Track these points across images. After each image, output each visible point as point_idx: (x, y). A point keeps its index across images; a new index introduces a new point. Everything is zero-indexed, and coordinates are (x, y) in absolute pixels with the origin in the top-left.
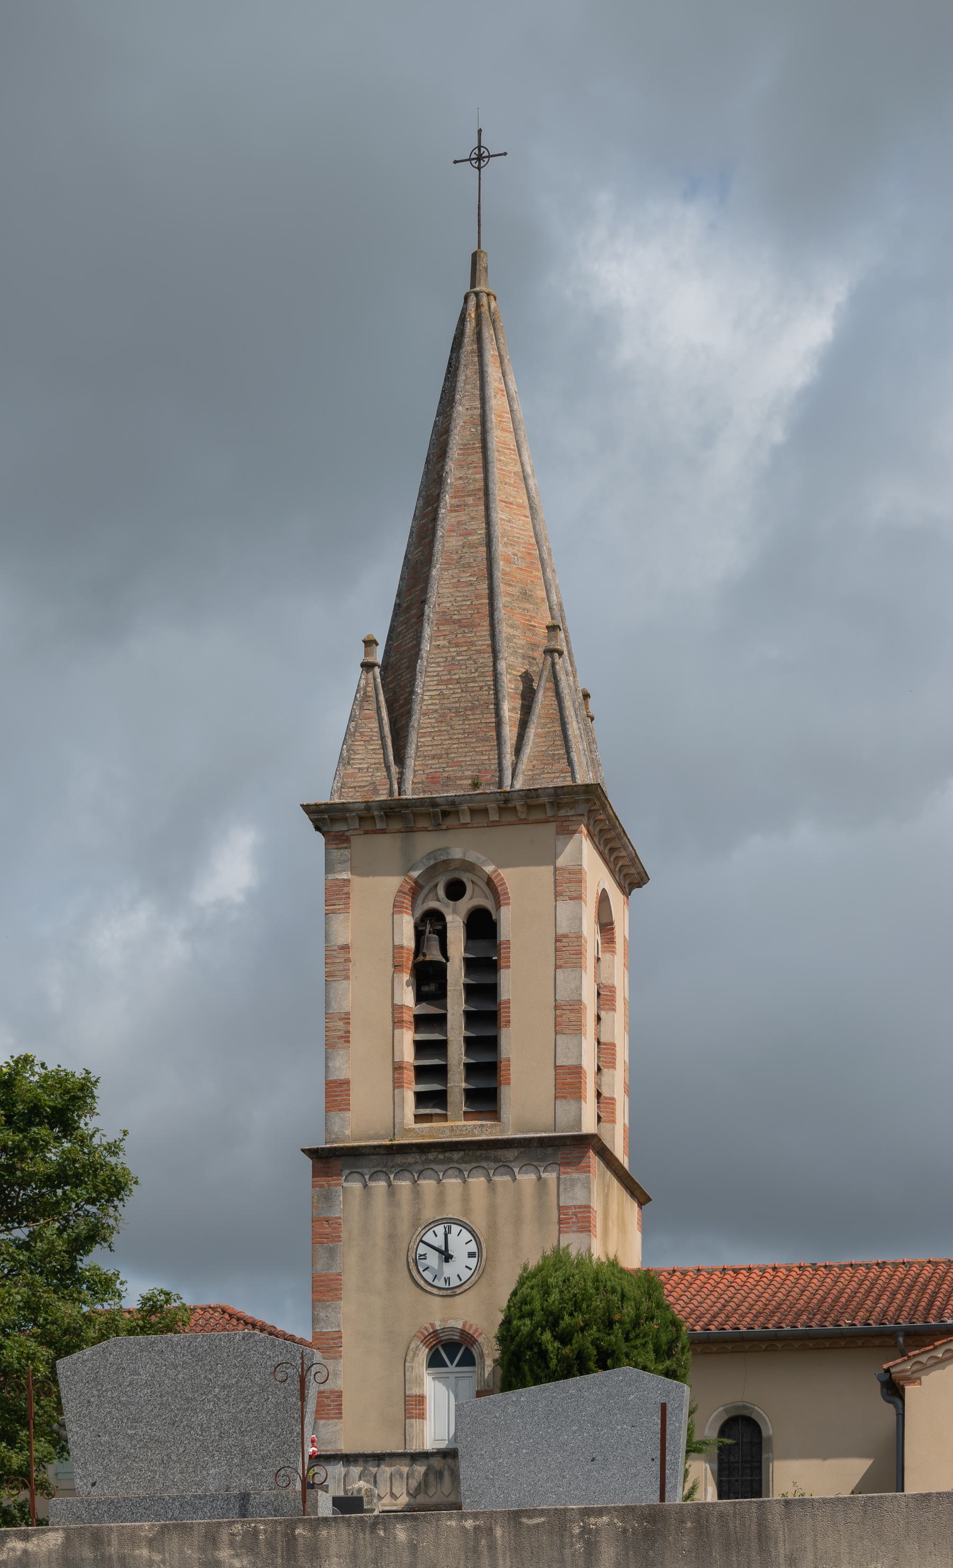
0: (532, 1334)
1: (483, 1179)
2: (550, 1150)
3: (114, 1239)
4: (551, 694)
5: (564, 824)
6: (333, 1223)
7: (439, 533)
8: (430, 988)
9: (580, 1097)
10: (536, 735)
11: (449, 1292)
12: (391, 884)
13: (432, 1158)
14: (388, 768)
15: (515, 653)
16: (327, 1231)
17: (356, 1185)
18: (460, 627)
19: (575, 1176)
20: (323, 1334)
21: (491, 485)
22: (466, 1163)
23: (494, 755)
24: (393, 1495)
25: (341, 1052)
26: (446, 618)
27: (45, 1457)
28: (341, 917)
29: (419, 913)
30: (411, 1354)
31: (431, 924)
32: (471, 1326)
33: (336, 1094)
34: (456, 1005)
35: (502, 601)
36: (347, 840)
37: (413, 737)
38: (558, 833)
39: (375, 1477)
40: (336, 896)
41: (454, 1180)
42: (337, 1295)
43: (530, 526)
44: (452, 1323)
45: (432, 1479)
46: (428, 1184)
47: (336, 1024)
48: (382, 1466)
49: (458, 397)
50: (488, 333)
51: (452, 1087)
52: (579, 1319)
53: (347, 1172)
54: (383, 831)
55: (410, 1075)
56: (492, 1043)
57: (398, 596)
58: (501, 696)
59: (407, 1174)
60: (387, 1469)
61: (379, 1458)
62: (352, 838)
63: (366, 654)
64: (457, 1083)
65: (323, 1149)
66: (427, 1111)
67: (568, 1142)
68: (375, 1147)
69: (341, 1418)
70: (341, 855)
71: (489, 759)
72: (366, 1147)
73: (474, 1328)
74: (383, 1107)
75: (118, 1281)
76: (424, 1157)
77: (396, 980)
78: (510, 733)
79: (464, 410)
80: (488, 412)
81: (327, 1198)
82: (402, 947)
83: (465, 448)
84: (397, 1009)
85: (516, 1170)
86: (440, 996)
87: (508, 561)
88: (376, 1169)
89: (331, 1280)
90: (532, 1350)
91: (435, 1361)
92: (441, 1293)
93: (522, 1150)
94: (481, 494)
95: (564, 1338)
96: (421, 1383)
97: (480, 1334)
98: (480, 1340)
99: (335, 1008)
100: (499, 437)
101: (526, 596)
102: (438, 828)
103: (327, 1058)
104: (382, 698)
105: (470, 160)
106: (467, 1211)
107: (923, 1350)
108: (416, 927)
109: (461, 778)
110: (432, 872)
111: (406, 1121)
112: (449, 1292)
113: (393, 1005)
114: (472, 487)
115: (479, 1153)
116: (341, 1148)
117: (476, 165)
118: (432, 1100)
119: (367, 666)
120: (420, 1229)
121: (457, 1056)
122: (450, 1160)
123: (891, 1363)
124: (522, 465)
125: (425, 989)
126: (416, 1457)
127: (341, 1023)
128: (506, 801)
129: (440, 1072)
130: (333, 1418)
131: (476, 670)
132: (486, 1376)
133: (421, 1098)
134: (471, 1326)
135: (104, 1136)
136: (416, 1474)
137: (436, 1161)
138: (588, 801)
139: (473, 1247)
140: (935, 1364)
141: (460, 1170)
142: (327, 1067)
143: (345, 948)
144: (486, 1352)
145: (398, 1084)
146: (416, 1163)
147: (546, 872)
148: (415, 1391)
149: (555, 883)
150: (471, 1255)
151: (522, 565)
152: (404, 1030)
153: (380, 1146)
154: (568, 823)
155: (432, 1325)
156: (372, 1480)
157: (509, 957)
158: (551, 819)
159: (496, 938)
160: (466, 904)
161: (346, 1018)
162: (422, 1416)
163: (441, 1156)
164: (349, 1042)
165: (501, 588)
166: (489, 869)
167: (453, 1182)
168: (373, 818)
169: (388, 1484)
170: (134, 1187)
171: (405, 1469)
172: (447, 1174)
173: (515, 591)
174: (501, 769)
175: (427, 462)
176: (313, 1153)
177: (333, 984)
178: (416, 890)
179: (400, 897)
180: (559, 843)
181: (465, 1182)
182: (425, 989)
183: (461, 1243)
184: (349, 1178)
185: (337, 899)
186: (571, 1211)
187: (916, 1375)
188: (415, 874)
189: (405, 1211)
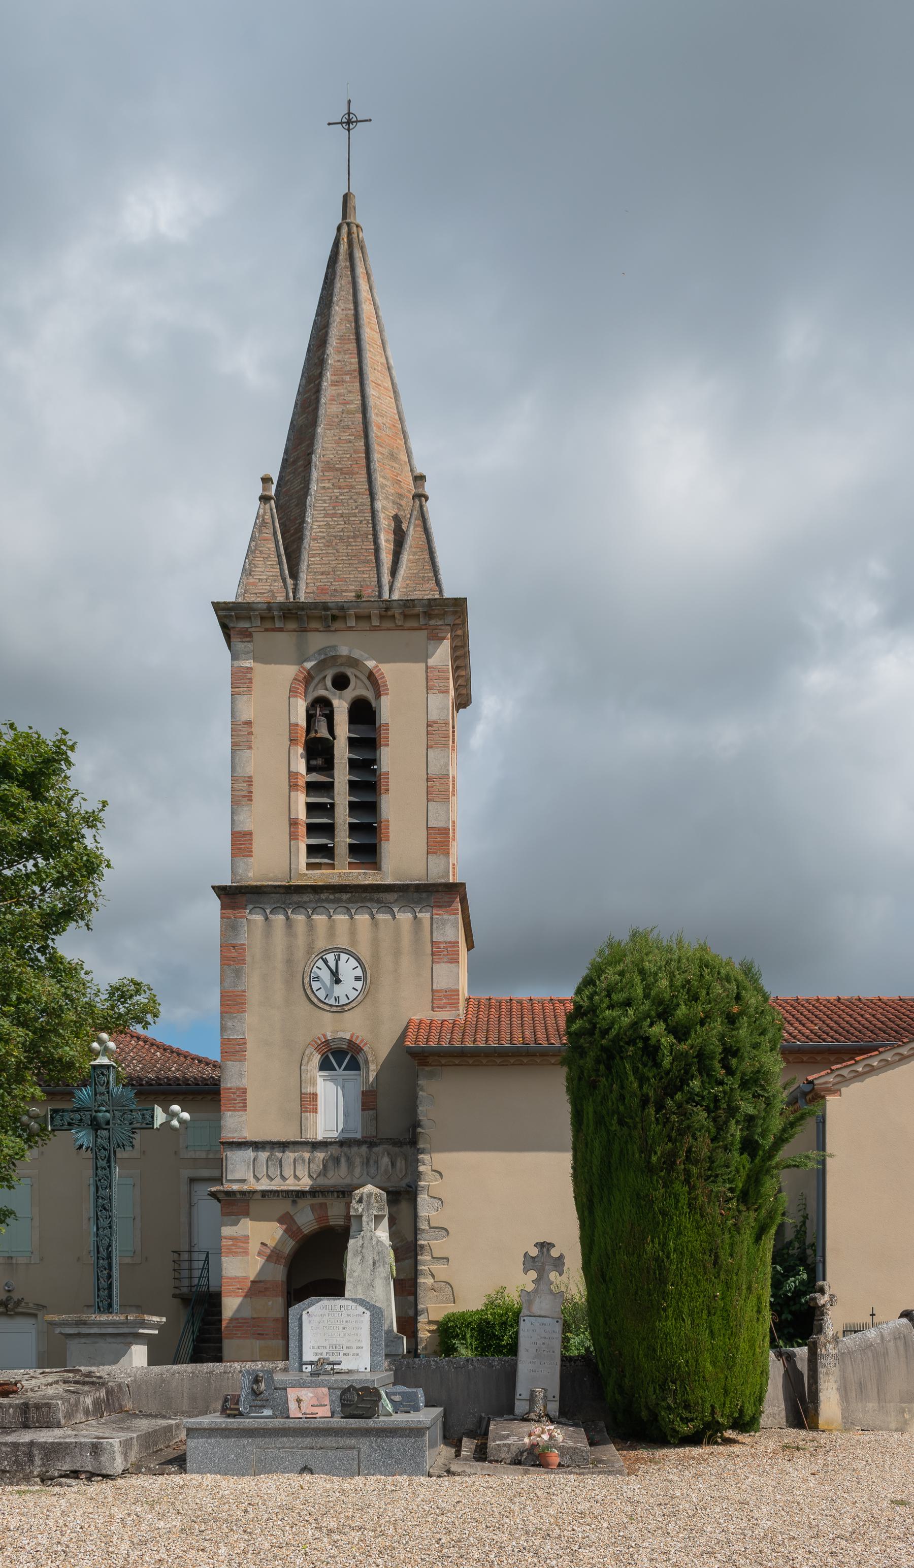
0: (635, 1025)
1: (367, 916)
2: (424, 895)
3: (94, 916)
4: (420, 529)
6: (240, 949)
7: (323, 401)
8: (319, 762)
9: (449, 853)
10: (409, 560)
11: (338, 1009)
12: (289, 671)
14: (284, 580)
15: (387, 498)
17: (258, 918)
18: (342, 473)
19: (446, 916)
20: (229, 1040)
21: (365, 367)
23: (374, 574)
24: (296, 1177)
26: (329, 467)
27: (17, 1154)
28: (245, 698)
29: (310, 698)
30: (306, 1059)
31: (320, 708)
33: (241, 843)
34: (342, 776)
35: (376, 457)
36: (250, 635)
37: (305, 556)
38: (429, 639)
40: (241, 681)
43: (394, 405)
44: (341, 1035)
45: (330, 1164)
46: (320, 919)
49: (335, 299)
50: (358, 254)
52: (699, 1010)
53: (251, 906)
54: (281, 630)
55: (302, 830)
56: (372, 807)
57: (286, 452)
58: (378, 528)
59: (303, 910)
60: (291, 1154)
61: (284, 1146)
62: (254, 634)
63: (263, 490)
64: (343, 839)
65: (230, 887)
66: (317, 860)
67: (440, 889)
68: (275, 887)
69: (246, 1110)
71: (369, 577)
72: (268, 886)
73: (360, 1039)
74: (280, 855)
75: (83, 972)
76: (317, 897)
77: (292, 751)
78: (386, 558)
79: (340, 310)
80: (360, 312)
82: (297, 725)
83: (341, 338)
84: (293, 775)
86: (328, 766)
87: (379, 428)
90: (635, 1044)
91: (325, 1066)
94: (357, 374)
95: (680, 1032)
96: (314, 1084)
97: (366, 1044)
98: (365, 1049)
99: (239, 772)
100: (369, 333)
101: (393, 456)
102: (327, 629)
103: (232, 813)
104: (277, 524)
105: (341, 123)
106: (353, 942)
107: (844, 1064)
108: (307, 711)
109: (346, 591)
110: (322, 665)
111: (301, 868)
112: (338, 1009)
113: (290, 772)
114: (348, 368)
115: (364, 895)
116: (247, 887)
117: (351, 116)
118: (320, 852)
119: (264, 499)
121: (342, 817)
122: (339, 900)
123: (815, 1076)
124: (387, 358)
125: (313, 762)
126: (315, 1146)
127: (245, 785)
128: (387, 609)
129: (328, 830)
131: (357, 508)
132: (371, 1079)
133: (312, 850)
134: (358, 1037)
135: (84, 799)
137: (327, 901)
138: (455, 613)
139: (359, 972)
140: (854, 1077)
142: (233, 820)
143: (249, 723)
144: (370, 1059)
145: (293, 836)
146: (310, 901)
147: (418, 669)
148: (309, 1090)
149: (427, 679)
150: (357, 979)
151: (388, 432)
152: (299, 793)
153: (280, 886)
154: (437, 631)
155: (324, 1036)
156: (278, 1164)
159: (375, 724)
160: (351, 693)
161: (249, 781)
162: (315, 1110)
163: (332, 897)
164: (251, 800)
165: (375, 447)
166: (371, 664)
167: (341, 918)
168: (273, 618)
169: (292, 1167)
170: (106, 871)
171: (307, 1155)
173: (385, 451)
174: (380, 586)
176: (221, 891)
177: (238, 752)
178: (308, 679)
180: (430, 648)
181: (352, 918)
182: (313, 762)
183: (348, 968)
186: (442, 946)
187: (836, 1087)
188: (309, 665)
189: (301, 941)
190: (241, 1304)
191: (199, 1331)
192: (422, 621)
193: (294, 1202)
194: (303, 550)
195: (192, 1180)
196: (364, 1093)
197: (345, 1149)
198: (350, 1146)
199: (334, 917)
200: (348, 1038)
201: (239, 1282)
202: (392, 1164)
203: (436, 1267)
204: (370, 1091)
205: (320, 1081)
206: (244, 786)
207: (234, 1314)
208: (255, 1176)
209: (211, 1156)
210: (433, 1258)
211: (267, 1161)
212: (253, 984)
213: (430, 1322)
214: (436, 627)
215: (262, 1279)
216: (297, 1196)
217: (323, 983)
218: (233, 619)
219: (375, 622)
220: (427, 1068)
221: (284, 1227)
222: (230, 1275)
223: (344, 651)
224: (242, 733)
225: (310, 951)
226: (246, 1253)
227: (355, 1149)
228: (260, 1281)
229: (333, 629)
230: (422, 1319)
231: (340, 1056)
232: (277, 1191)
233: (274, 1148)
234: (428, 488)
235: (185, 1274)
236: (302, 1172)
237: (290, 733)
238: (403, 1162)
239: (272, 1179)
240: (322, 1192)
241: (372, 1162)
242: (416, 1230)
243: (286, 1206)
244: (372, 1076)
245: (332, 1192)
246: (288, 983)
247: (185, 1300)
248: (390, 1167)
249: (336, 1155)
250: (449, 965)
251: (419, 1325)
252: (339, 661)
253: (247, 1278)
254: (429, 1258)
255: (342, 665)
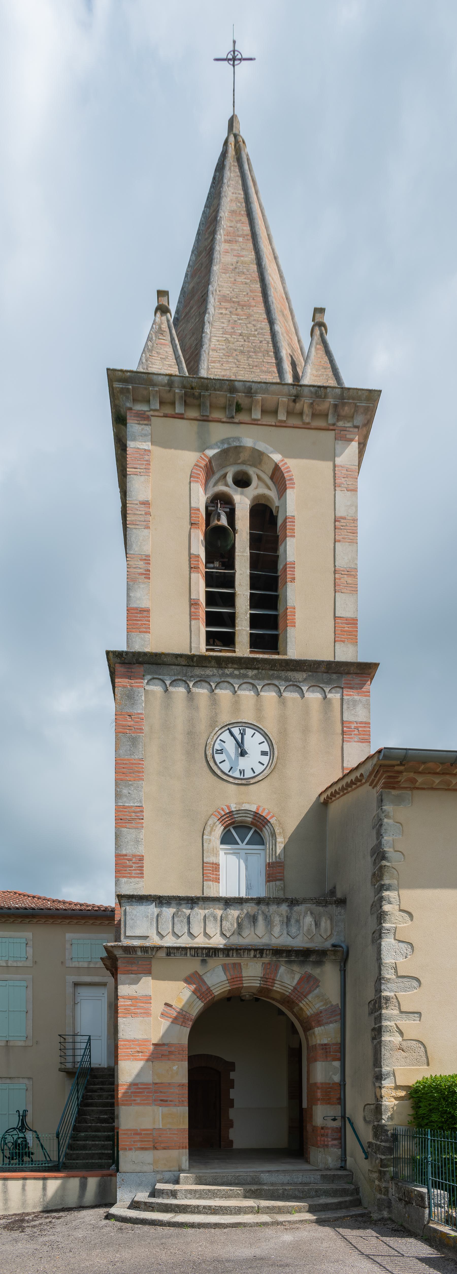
1: (274, 694)
2: (334, 676)
4: (322, 352)
5: (342, 432)
11: (243, 782)
13: (228, 673)
16: (129, 723)
17: (156, 689)
19: (357, 698)
22: (259, 679)
24: (206, 935)
25: (142, 586)
29: (210, 493)
30: (208, 829)
31: (221, 502)
32: (264, 809)
33: (137, 618)
36: (148, 418)
39: (189, 918)
41: (247, 693)
42: (139, 776)
45: (246, 923)
46: (224, 693)
47: (137, 563)
48: (196, 909)
51: (239, 630)
53: (149, 677)
54: (181, 417)
59: (204, 684)
60: (201, 911)
61: (192, 901)
64: (243, 629)
67: (352, 670)
69: (142, 877)
70: (142, 429)
73: (266, 811)
76: (221, 672)
81: (130, 697)
85: (305, 688)
88: (176, 678)
89: (132, 764)
91: (226, 839)
92: (236, 781)
93: (310, 673)
94: (250, 237)
96: (217, 855)
97: (273, 816)
98: (272, 821)
102: (231, 421)
103: (128, 589)
106: (260, 718)
113: (190, 554)
115: (271, 672)
120: (217, 729)
122: (245, 676)
126: (228, 902)
127: (142, 563)
130: (135, 877)
132: (278, 851)
136: (230, 917)
137: (232, 676)
139: (265, 747)
141: (253, 685)
142: (128, 596)
143: (146, 503)
146: (213, 675)
148: (212, 859)
150: (264, 753)
154: (346, 432)
155: (228, 807)
156: (185, 920)
157: (293, 529)
158: (331, 427)
160: (256, 489)
161: (146, 559)
162: (217, 880)
163: (236, 672)
164: (149, 578)
166: (277, 457)
171: (219, 913)
172: (241, 687)
175: (198, 234)
178: (210, 471)
179: (196, 469)
181: (258, 694)
183: (254, 743)
184: (151, 683)
185: (139, 464)
188: (211, 453)
190: (142, 1069)
191: (83, 1097)
192: (331, 420)
193: (204, 961)
194: (203, 353)
195: (76, 985)
196: (269, 865)
197: (263, 907)
198: (268, 904)
199: (239, 692)
200: (254, 810)
201: (139, 1045)
202: (316, 925)
203: (405, 1023)
204: (276, 862)
205: (222, 853)
206: (141, 563)
207: (138, 1075)
208: (159, 933)
209: (92, 965)
210: (401, 1012)
211: (173, 917)
212: (151, 753)
213: (397, 1087)
214: (344, 429)
215: (165, 1042)
216: (208, 955)
217: (228, 756)
218: (129, 394)
219: (282, 416)
220: (394, 792)
221: (193, 987)
222: (128, 1037)
223: (248, 442)
224: (140, 513)
225: (213, 723)
226: (147, 1014)
227: (273, 908)
228: (164, 1045)
229: (236, 420)
230: (387, 1083)
231: (245, 829)
232: (185, 949)
233: (180, 904)
234: (327, 319)
235: (70, 1052)
236: (213, 929)
237: (191, 517)
238: (329, 922)
239: (178, 937)
240: (237, 950)
241: (293, 921)
242: (379, 980)
243: (193, 965)
244: (279, 848)
245: (249, 950)
246: (189, 755)
247: (70, 1073)
248: (313, 927)
249: (252, 914)
250: (360, 744)
251: (384, 1091)
252: (244, 456)
253: (147, 1041)
254: (396, 1012)
255: (243, 463)
